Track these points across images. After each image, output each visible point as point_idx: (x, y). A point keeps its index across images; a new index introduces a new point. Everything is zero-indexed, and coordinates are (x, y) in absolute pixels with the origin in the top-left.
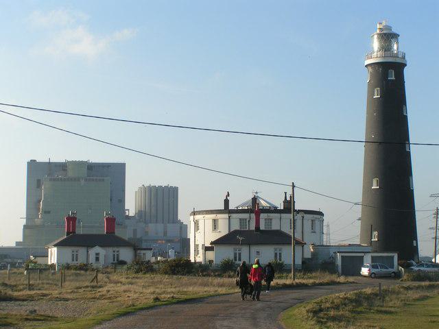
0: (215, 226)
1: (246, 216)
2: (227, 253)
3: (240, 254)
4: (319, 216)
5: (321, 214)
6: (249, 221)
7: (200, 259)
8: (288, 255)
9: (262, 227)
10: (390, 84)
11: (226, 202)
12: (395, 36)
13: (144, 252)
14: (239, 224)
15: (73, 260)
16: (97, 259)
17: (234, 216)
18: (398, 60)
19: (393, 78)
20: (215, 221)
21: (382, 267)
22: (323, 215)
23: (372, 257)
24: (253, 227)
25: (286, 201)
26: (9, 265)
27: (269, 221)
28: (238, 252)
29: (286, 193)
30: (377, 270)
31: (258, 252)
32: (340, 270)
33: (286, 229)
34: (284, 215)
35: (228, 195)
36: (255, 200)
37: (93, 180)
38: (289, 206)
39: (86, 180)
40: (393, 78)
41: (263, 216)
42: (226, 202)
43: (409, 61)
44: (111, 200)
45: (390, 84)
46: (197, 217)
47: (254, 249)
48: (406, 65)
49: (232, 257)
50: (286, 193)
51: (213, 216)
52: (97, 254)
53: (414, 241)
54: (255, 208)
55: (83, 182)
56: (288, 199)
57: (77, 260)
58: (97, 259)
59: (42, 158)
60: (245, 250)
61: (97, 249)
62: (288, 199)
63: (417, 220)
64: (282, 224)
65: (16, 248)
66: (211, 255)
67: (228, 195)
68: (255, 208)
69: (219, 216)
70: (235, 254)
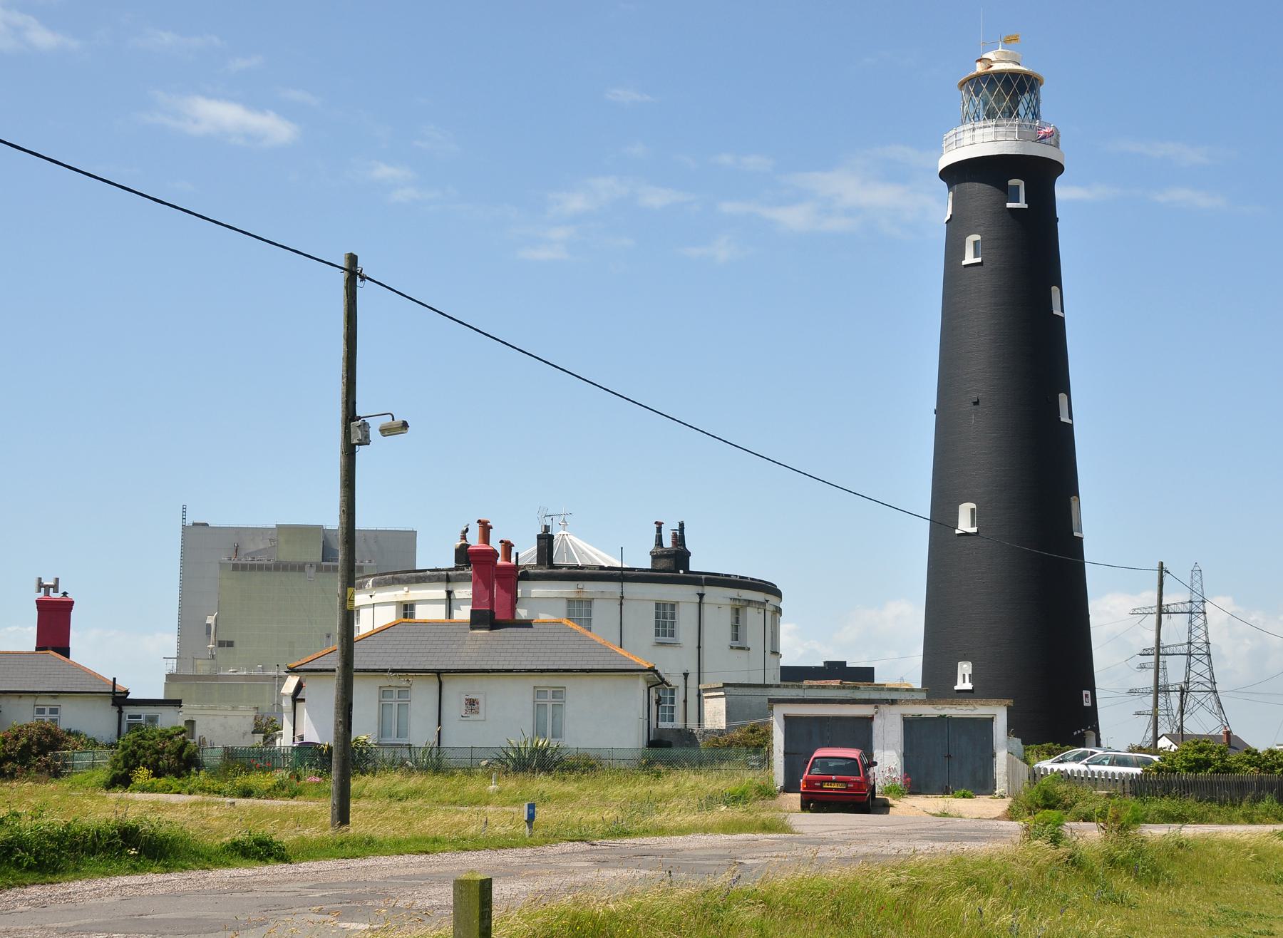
22: (778, 593)
29: (659, 526)
31: (472, 703)
50: (659, 526)
62: (668, 543)
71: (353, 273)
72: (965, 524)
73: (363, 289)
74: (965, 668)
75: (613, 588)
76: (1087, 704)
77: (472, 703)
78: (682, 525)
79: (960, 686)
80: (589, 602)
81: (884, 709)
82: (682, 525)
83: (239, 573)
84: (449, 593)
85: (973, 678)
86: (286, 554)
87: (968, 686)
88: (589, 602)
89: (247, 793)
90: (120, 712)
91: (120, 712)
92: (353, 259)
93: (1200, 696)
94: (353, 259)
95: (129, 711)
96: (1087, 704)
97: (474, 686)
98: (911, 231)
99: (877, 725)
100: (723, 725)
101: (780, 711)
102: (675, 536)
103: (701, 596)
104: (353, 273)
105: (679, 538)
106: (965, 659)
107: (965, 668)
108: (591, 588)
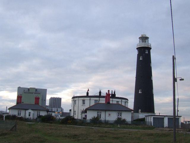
0: (84, 103)
2: (91, 115)
3: (20, 113)
6: (99, 101)
7: (80, 118)
10: (144, 56)
11: (88, 93)
12: (147, 38)
13: (52, 113)
15: (18, 115)
16: (29, 115)
17: (92, 99)
18: (149, 47)
19: (147, 53)
20: (84, 101)
23: (153, 118)
28: (19, 112)
29: (112, 91)
31: (110, 114)
32: (180, 127)
35: (88, 90)
39: (35, 93)
40: (147, 53)
42: (88, 93)
43: (152, 47)
44: (42, 100)
45: (144, 56)
46: (75, 99)
47: (107, 113)
48: (151, 48)
49: (96, 116)
50: (112, 91)
51: (83, 98)
52: (30, 113)
56: (113, 93)
57: (20, 115)
58: (29, 115)
59: (22, 86)
61: (30, 111)
62: (113, 93)
63: (133, 106)
66: (8, 111)
67: (88, 90)
69: (85, 98)
81: (166, 117)
83: (133, 57)
86: (30, 91)
95: (48, 113)
97: (110, 112)
106: (140, 109)
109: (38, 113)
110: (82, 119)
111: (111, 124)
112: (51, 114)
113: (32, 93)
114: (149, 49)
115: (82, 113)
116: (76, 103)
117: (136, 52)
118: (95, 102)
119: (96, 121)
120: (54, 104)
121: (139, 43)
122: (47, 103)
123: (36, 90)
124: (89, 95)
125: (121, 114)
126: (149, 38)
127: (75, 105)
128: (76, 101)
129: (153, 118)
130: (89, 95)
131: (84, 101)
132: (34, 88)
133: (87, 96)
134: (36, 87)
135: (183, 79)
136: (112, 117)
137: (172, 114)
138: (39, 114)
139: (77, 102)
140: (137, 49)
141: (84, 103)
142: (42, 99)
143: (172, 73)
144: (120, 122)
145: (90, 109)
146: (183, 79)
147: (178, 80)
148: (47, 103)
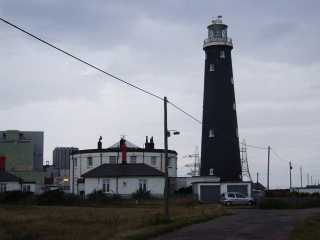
0: (90, 163)
1: (115, 154)
3: (108, 185)
4: (173, 155)
5: (175, 153)
6: (117, 159)
8: (156, 187)
9: (128, 161)
11: (100, 144)
14: (208, 35)
17: (104, 154)
18: (227, 44)
20: (90, 159)
21: (238, 196)
22: (176, 154)
23: (201, 186)
24: (120, 161)
25: (147, 144)
26: (67, 180)
27: (134, 157)
29: (147, 137)
30: (233, 198)
31: (125, 183)
33: (148, 162)
34: (146, 154)
35: (101, 138)
36: (123, 142)
37: (22, 142)
38: (150, 146)
39: (18, 142)
41: (129, 154)
42: (100, 144)
44: (34, 155)
47: (121, 181)
48: (232, 48)
49: (100, 187)
50: (147, 137)
51: (88, 155)
53: (240, 176)
54: (123, 147)
55: (16, 143)
60: (113, 182)
62: (149, 142)
64: (146, 159)
65: (6, 181)
67: (101, 138)
68: (123, 147)
70: (104, 185)
71: (166, 100)
72: (211, 135)
73: (168, 104)
74: (211, 170)
75: (141, 154)
76: (241, 178)
77: (125, 183)
78: (152, 137)
79: (210, 174)
80: (136, 157)
82: (152, 137)
84: (101, 155)
85: (214, 172)
87: (213, 174)
88: (136, 157)
89: (139, 208)
90: (21, 185)
91: (21, 185)
92: (165, 98)
93: (245, 173)
94: (165, 98)
96: (241, 178)
98: (202, 36)
99: (222, 187)
100: (51, 164)
101: (199, 185)
102: (151, 140)
103: (162, 155)
104: (166, 100)
105: (152, 140)
106: (211, 168)
107: (211, 170)
108: (136, 153)
109: (4, 186)
110: (79, 193)
111: (128, 200)
112: (29, 187)
113: (13, 142)
114: (228, 49)
115: (78, 183)
116: (76, 164)
117: (203, 56)
118: (131, 159)
119: (99, 197)
120: (63, 161)
121: (208, 37)
122: (48, 158)
123: (21, 134)
124: (103, 147)
125: (5, 185)
126: (227, 27)
127: (75, 167)
128: (76, 159)
129: (201, 186)
130: (103, 147)
131: (90, 159)
132: (17, 131)
133: (100, 149)
134: (21, 130)
135: (178, 133)
136: (128, 187)
137: (243, 180)
138: (5, 188)
139: (78, 160)
140: (204, 49)
141: (90, 163)
142: (34, 153)
143: (168, 125)
144: (142, 195)
145: (92, 174)
146: (178, 133)
147: (172, 133)
148: (48, 158)
